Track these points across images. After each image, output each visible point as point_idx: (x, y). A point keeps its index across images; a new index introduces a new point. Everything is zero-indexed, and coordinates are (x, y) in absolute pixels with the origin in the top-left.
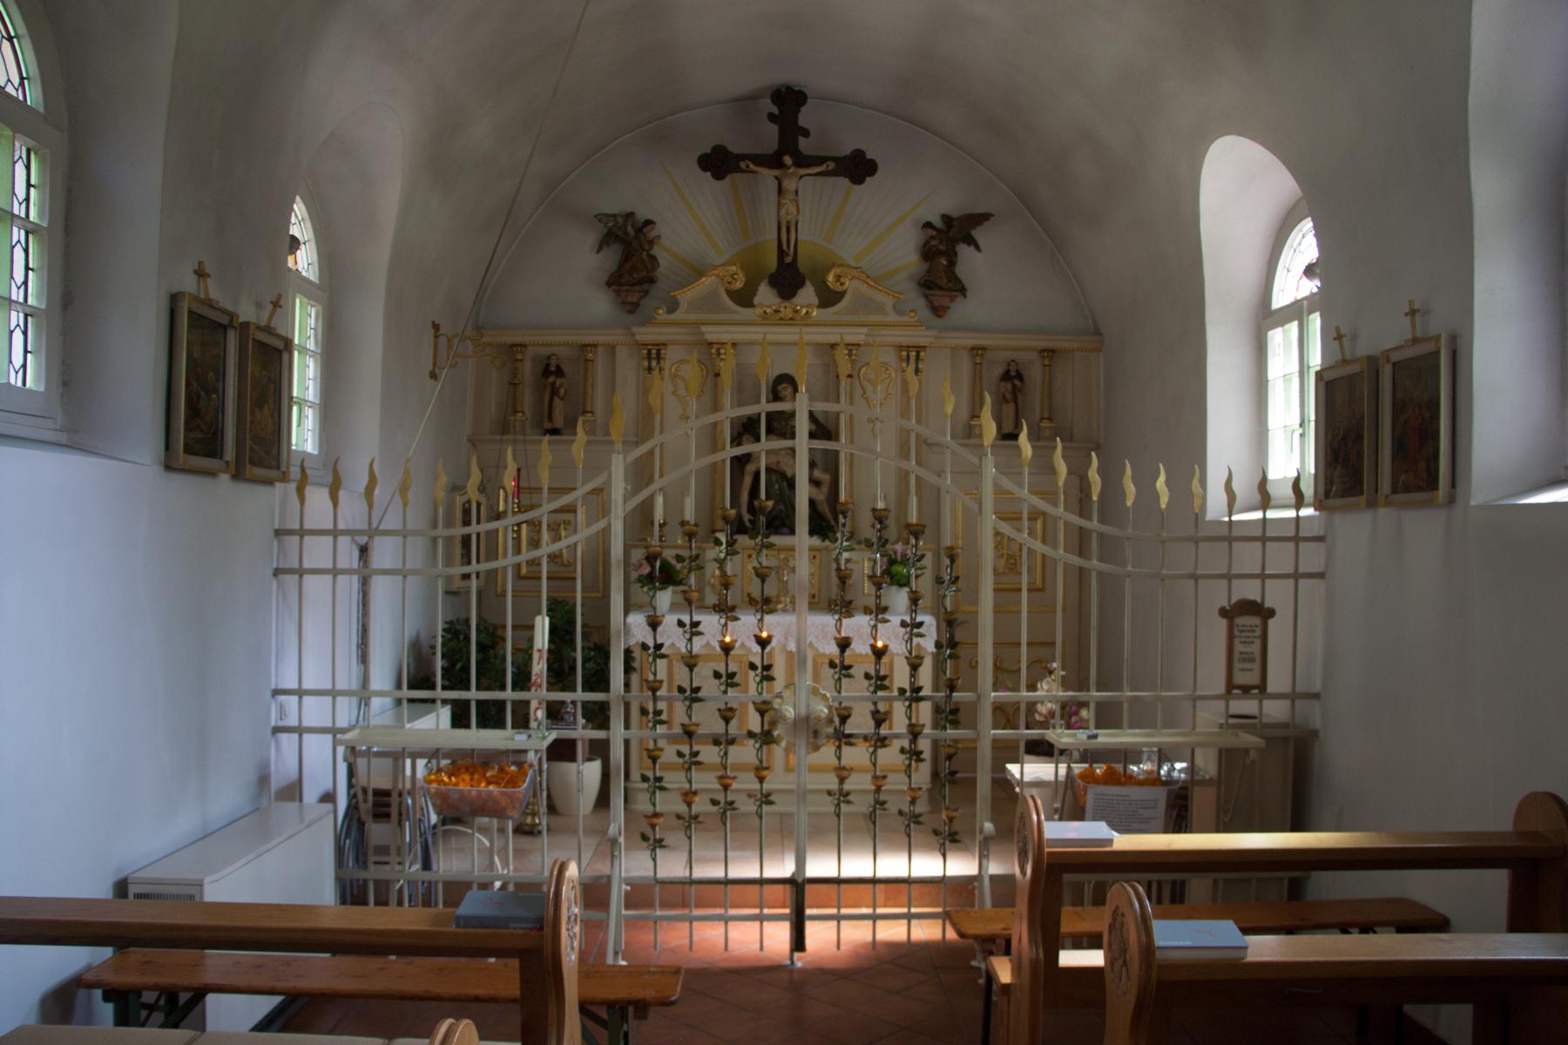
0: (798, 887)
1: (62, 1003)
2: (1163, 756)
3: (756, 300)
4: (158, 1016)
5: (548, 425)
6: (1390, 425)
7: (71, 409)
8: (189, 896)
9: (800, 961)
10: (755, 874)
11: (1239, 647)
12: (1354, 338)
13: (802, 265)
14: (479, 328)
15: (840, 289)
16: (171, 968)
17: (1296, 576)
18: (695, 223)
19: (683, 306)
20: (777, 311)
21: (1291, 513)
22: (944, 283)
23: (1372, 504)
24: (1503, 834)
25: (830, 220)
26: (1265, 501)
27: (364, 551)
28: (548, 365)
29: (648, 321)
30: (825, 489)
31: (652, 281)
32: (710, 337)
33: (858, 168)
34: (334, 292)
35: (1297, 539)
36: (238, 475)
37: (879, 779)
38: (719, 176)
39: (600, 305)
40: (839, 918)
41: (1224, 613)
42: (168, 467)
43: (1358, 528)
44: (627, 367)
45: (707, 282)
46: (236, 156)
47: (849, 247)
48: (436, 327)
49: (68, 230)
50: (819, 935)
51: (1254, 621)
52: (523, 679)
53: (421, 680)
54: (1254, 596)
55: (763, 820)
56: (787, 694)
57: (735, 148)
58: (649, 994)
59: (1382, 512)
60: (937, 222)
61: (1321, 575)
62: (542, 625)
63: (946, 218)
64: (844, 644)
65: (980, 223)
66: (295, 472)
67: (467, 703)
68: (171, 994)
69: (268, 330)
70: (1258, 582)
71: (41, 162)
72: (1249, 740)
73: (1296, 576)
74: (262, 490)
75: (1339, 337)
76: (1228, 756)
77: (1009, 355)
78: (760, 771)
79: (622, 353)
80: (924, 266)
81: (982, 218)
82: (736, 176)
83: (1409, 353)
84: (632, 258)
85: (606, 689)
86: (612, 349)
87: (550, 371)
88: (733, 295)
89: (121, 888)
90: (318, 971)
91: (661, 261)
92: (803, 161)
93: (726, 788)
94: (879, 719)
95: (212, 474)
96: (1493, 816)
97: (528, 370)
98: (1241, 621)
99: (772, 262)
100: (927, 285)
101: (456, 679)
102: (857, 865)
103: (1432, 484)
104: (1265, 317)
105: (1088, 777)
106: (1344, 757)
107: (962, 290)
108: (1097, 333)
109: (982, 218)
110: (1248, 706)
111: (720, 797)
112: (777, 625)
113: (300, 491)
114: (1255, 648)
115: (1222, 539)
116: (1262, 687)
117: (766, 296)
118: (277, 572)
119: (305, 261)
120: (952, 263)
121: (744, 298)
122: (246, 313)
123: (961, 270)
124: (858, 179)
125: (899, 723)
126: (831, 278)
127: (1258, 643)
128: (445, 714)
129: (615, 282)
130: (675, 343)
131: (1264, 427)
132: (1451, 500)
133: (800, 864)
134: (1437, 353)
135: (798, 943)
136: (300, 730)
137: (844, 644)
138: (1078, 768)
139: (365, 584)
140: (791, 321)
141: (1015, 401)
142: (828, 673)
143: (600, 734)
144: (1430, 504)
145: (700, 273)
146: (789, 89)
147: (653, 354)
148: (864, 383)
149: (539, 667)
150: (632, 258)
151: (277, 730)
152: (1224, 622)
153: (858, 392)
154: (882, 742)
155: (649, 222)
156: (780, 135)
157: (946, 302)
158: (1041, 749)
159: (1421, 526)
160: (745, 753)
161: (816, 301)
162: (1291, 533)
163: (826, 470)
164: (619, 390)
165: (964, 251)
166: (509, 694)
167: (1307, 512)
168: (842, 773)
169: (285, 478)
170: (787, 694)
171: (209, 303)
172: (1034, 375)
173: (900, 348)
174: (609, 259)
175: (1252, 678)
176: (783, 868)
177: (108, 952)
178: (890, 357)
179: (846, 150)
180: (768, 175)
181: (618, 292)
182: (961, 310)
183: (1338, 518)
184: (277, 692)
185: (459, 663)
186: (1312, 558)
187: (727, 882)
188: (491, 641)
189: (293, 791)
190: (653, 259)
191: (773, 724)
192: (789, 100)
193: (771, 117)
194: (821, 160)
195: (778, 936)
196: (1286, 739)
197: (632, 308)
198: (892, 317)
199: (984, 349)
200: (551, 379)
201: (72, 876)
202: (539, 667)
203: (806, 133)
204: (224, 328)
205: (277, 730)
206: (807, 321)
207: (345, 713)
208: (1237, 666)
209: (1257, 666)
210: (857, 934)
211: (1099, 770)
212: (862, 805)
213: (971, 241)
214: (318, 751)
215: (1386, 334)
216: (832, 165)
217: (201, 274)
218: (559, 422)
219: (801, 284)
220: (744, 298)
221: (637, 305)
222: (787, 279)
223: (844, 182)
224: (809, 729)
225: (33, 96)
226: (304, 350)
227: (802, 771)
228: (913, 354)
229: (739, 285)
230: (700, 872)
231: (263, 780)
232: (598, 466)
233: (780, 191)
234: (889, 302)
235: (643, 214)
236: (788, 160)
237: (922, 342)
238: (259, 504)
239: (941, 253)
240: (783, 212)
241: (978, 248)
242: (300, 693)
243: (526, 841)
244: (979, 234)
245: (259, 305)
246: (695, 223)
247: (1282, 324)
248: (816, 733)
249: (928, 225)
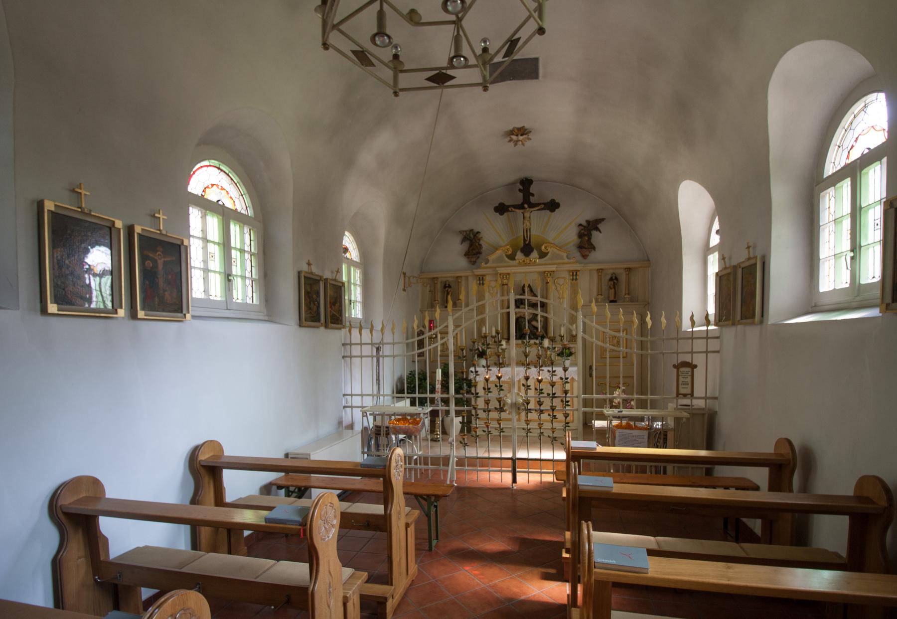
0: (514, 460)
1: (267, 489)
2: (654, 419)
4: (295, 495)
6: (742, 290)
7: (269, 309)
8: (306, 457)
9: (515, 487)
10: (499, 456)
11: (681, 380)
12: (730, 258)
13: (532, 244)
14: (422, 272)
16: (299, 480)
17: (707, 352)
18: (495, 231)
19: (491, 261)
21: (705, 328)
23: (733, 324)
24: (770, 454)
25: (539, 225)
26: (708, 323)
27: (378, 349)
29: (479, 267)
31: (480, 253)
33: (553, 206)
34: (365, 265)
35: (707, 338)
36: (326, 327)
37: (540, 425)
38: (501, 214)
39: (463, 262)
40: (528, 472)
41: (675, 366)
42: (300, 326)
43: (730, 333)
44: (474, 286)
45: (499, 252)
46: (319, 222)
47: (551, 236)
48: (404, 274)
49: (264, 253)
50: (522, 478)
51: (689, 369)
52: (433, 391)
53: (400, 391)
54: (689, 360)
55: (502, 438)
56: (508, 395)
57: (507, 203)
58: (440, 493)
59: (739, 327)
60: (584, 223)
61: (718, 352)
62: (439, 372)
63: (588, 222)
64: (527, 378)
66: (348, 324)
67: (415, 398)
68: (300, 489)
69: (335, 280)
70: (690, 355)
71: (254, 232)
72: (685, 414)
73: (707, 352)
74: (337, 332)
75: (724, 259)
76: (677, 420)
77: (612, 271)
78: (499, 421)
79: (470, 279)
80: (579, 240)
81: (601, 220)
82: (510, 213)
83: (747, 264)
84: (473, 246)
85: (448, 393)
86: (467, 277)
87: (447, 286)
89: (287, 455)
90: (356, 482)
91: (484, 246)
92: (532, 206)
93: (487, 427)
94: (540, 403)
95: (318, 327)
96: (767, 448)
97: (439, 286)
98: (682, 369)
99: (522, 244)
100: (580, 247)
101: (411, 390)
102: (534, 454)
103: (753, 316)
104: (707, 249)
105: (619, 427)
106: (726, 422)
107: (594, 248)
108: (648, 260)
109: (601, 220)
110: (687, 401)
111: (486, 429)
112: (506, 373)
113: (350, 331)
114: (689, 380)
115: (688, 338)
116: (692, 394)
117: (520, 256)
118: (343, 357)
119: (354, 254)
120: (590, 239)
121: (512, 257)
122: (327, 275)
123: (593, 241)
124: (553, 210)
125: (547, 405)
126: (543, 248)
127: (690, 378)
128: (408, 401)
129: (467, 254)
131: (698, 295)
132: (761, 322)
133: (514, 453)
134: (756, 264)
135: (514, 480)
136: (352, 407)
137: (527, 378)
138: (615, 423)
139: (378, 361)
140: (529, 265)
142: (523, 388)
143: (447, 408)
144: (753, 324)
145: (496, 249)
146: (527, 179)
147: (481, 279)
149: (438, 386)
150: (473, 246)
151: (344, 407)
152: (675, 370)
154: (542, 412)
155: (478, 232)
156: (525, 196)
157: (587, 253)
158: (602, 417)
159: (752, 333)
160: (494, 415)
162: (705, 335)
165: (595, 233)
166: (428, 395)
167: (711, 328)
168: (527, 422)
169: (344, 327)
170: (508, 395)
171: (312, 273)
172: (623, 278)
173: (570, 271)
174: (465, 247)
175: (688, 391)
176: (510, 455)
177: (283, 474)
178: (566, 275)
179: (548, 200)
180: (519, 212)
182: (593, 256)
183: (724, 329)
184: (344, 395)
185: (412, 385)
186: (713, 345)
187: (501, 459)
188: (423, 378)
189: (351, 427)
190: (480, 245)
191: (504, 405)
192: (526, 183)
193: (520, 190)
194: (540, 204)
195: (507, 478)
196: (703, 414)
197: (474, 263)
201: (273, 452)
202: (438, 386)
203: (533, 195)
204: (319, 281)
205: (344, 407)
206: (535, 264)
207: (368, 402)
208: (681, 386)
209: (689, 386)
210: (535, 479)
211: (624, 422)
212: (535, 433)
213: (597, 229)
214: (358, 413)
215: (740, 257)
216: (543, 206)
217: (309, 264)
219: (532, 251)
220: (512, 257)
222: (527, 249)
223: (548, 212)
224: (516, 407)
225: (250, 213)
226: (355, 285)
227: (514, 422)
228: (574, 274)
229: (510, 253)
230: (493, 455)
231: (340, 423)
232: (444, 319)
233: (524, 218)
234: (565, 255)
235: (476, 230)
236: (526, 206)
238: (336, 336)
239: (585, 235)
242: (352, 395)
243: (434, 443)
244: (600, 226)
245: (332, 272)
246: (495, 231)
247: (713, 253)
248: (519, 409)
249: (580, 225)
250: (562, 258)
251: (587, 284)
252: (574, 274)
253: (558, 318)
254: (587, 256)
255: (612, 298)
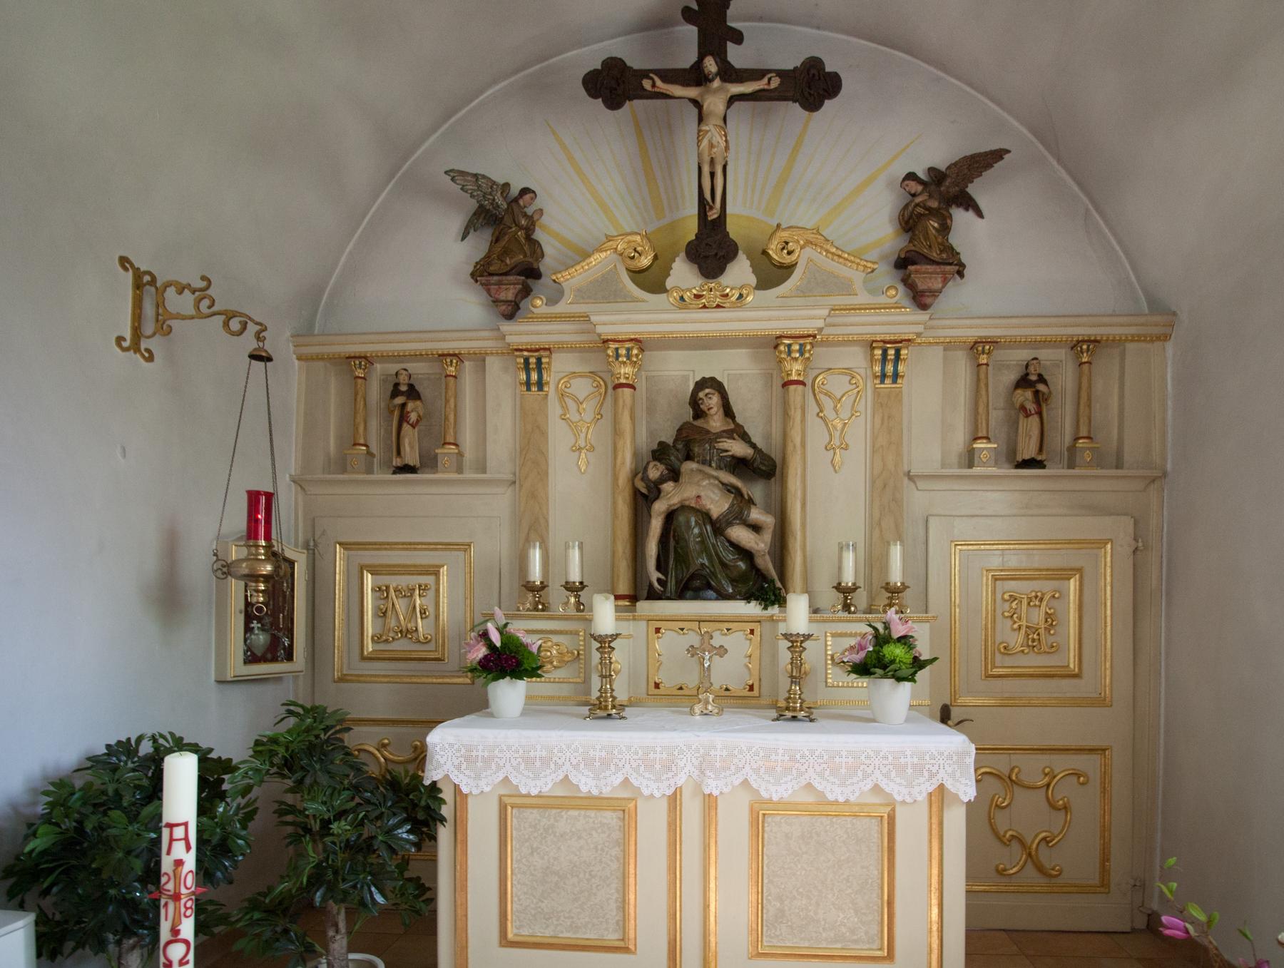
3: (669, 283)
5: (397, 462)
13: (734, 229)
15: (788, 260)
18: (591, 189)
20: (698, 297)
22: (934, 255)
28: (397, 385)
30: (767, 536)
32: (605, 331)
33: (812, 86)
38: (614, 103)
44: (501, 383)
47: (801, 213)
57: (635, 63)
60: (922, 175)
63: (931, 170)
65: (989, 166)
79: (493, 364)
84: (510, 251)
87: (404, 392)
88: (637, 275)
91: (547, 249)
97: (375, 392)
99: (691, 229)
107: (961, 274)
117: (683, 275)
120: (945, 229)
123: (956, 239)
130: (563, 347)
141: (1040, 414)
147: (533, 364)
148: (822, 397)
150: (510, 251)
153: (812, 408)
161: (752, 280)
163: (768, 510)
164: (490, 412)
172: (1063, 380)
173: (871, 346)
178: (855, 359)
181: (487, 286)
198: (863, 298)
199: (994, 342)
200: (400, 400)
213: (969, 203)
218: (411, 457)
220: (651, 280)
221: (516, 307)
222: (712, 248)
228: (889, 355)
229: (645, 261)
237: (906, 331)
240: (705, 143)
241: (980, 214)
249: (911, 176)
250: (846, 288)
251: (935, 402)
252: (889, 355)
253: (830, 510)
254: (935, 293)
255: (1028, 450)
